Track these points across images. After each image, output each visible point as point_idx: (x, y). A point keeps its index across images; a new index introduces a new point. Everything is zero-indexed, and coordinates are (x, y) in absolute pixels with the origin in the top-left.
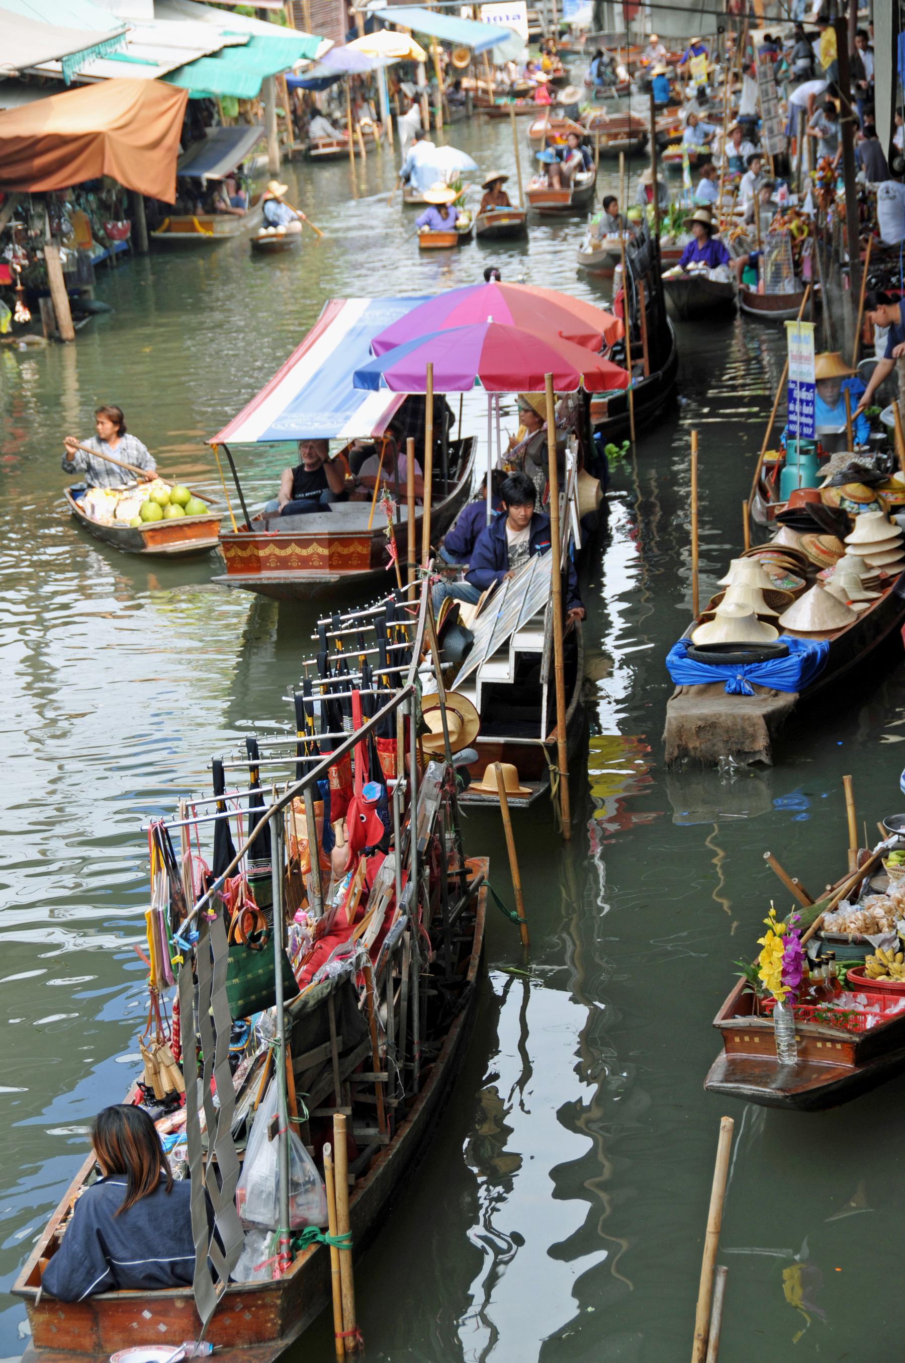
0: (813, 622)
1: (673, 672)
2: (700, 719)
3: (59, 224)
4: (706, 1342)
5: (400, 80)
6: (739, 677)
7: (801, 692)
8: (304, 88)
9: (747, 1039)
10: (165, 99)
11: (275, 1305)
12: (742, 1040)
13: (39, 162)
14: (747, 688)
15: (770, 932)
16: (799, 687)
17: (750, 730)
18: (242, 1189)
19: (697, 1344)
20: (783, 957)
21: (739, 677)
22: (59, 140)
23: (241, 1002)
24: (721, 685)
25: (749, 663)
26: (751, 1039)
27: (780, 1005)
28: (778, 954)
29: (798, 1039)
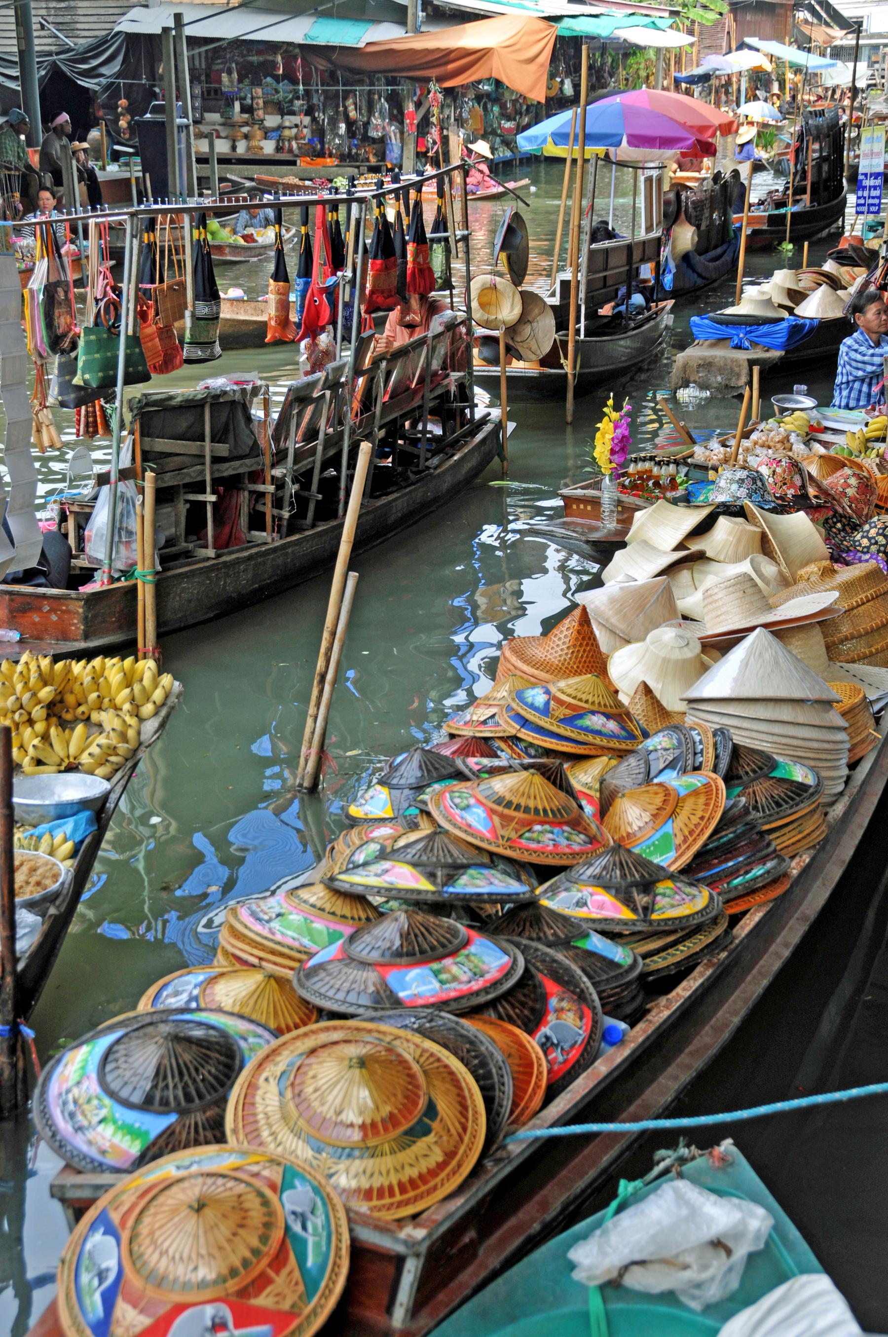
0: (818, 311)
1: (694, 329)
2: (701, 359)
3: (461, 113)
4: (333, 634)
5: (757, 88)
6: (741, 335)
7: (787, 352)
8: (686, 83)
9: (582, 506)
10: (541, 31)
11: (78, 612)
12: (578, 507)
13: (451, 67)
14: (747, 344)
15: (606, 419)
16: (785, 346)
17: (737, 370)
18: (91, 530)
19: (326, 635)
20: (613, 439)
21: (741, 335)
22: (467, 53)
23: (100, 374)
24: (728, 342)
25: (751, 325)
26: (585, 507)
27: (607, 479)
28: (609, 436)
29: (620, 509)
